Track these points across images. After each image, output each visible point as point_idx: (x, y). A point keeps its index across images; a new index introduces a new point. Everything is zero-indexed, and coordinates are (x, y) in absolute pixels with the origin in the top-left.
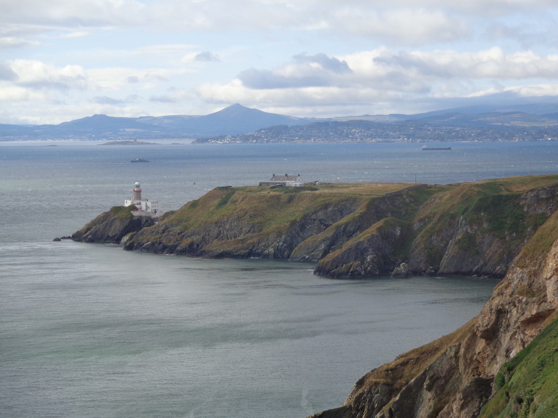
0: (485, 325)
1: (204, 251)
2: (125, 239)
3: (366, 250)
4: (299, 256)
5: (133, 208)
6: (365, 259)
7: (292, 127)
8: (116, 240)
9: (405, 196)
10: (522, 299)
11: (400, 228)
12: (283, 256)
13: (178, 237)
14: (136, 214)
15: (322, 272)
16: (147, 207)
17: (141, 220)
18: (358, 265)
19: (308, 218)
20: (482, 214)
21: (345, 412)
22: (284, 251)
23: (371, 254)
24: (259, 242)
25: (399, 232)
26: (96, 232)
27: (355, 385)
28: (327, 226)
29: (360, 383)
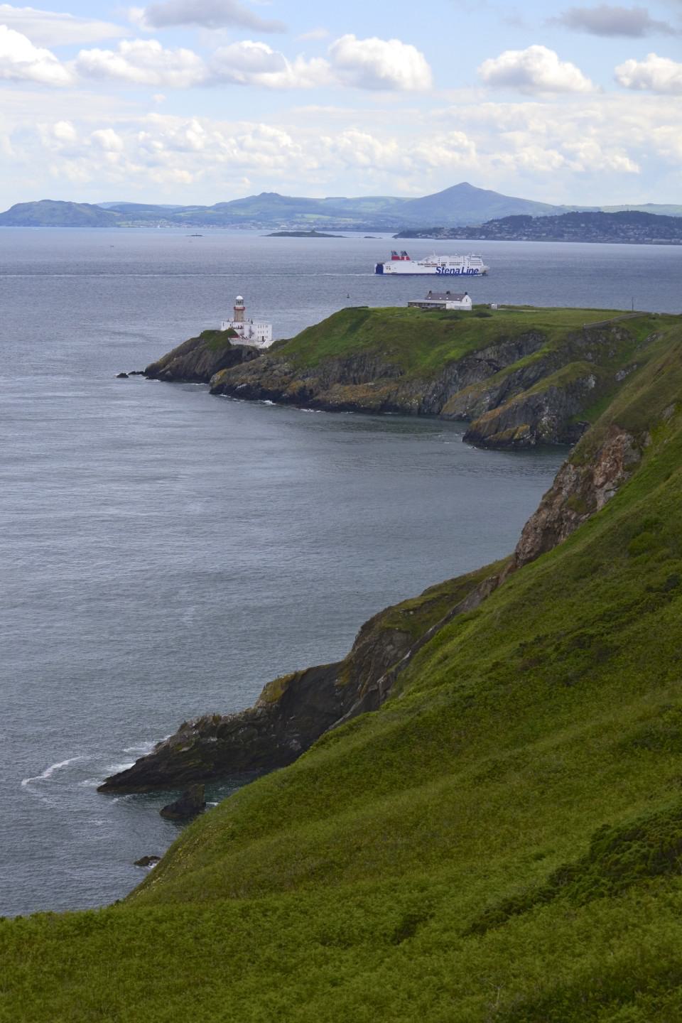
0: (527, 550)
2: (217, 377)
3: (540, 408)
5: (231, 333)
6: (540, 421)
7: (538, 219)
8: (204, 378)
10: (571, 515)
12: (428, 415)
14: (235, 342)
15: (474, 438)
17: (241, 351)
18: (526, 432)
21: (342, 670)
22: (434, 403)
23: (547, 414)
24: (397, 390)
25: (594, 383)
26: (178, 366)
27: (359, 629)
28: (498, 369)
29: (367, 628)
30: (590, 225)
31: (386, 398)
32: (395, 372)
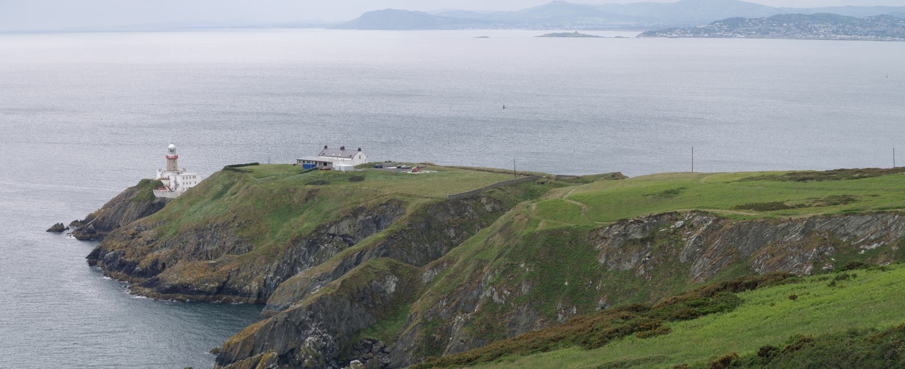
1: (158, 279)
4: (279, 303)
6: (302, 342)
7: (750, 20)
9: (484, 201)
11: (396, 279)
13: (146, 247)
14: (158, 194)
16: (177, 185)
19: (323, 231)
20: (522, 265)
24: (238, 270)
25: (394, 285)
26: (104, 218)
30: (791, 25)
31: (225, 279)
32: (243, 248)
